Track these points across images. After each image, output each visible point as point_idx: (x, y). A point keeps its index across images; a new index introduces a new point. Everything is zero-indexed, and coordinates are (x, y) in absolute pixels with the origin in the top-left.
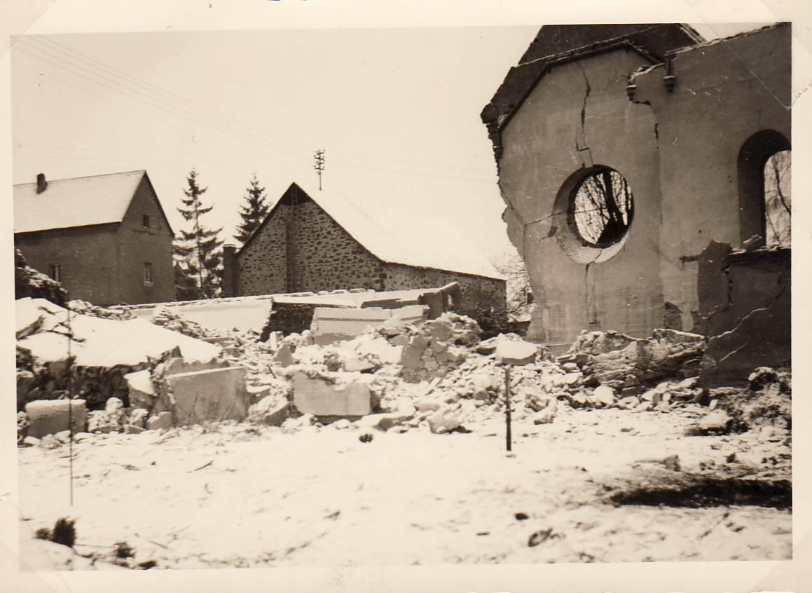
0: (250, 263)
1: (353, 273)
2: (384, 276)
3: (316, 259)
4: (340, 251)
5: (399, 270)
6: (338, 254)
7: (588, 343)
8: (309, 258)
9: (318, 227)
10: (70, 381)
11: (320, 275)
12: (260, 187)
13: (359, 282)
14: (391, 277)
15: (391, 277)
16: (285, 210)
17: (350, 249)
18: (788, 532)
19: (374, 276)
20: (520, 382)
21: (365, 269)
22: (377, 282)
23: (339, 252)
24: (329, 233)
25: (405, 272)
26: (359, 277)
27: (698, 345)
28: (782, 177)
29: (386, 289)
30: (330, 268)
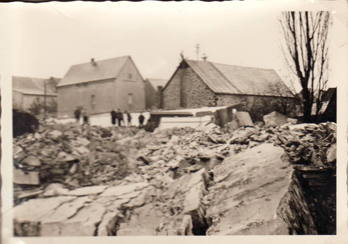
0: (168, 94)
1: (205, 98)
2: (217, 99)
3: (191, 92)
4: (201, 88)
5: (226, 96)
6: (200, 90)
7: (327, 163)
8: (189, 91)
9: (192, 78)
10: (298, 105)
11: (193, 99)
12: (206, 56)
13: (286, 93)
14: (221, 100)
15: (221, 100)
16: (180, 71)
17: (204, 87)
18: (96, 234)
19: (213, 100)
20: (112, 151)
21: (209, 96)
22: (214, 102)
23: (200, 89)
24: (196, 81)
25: (230, 96)
26: (207, 100)
27: (145, 191)
28: (101, 197)
29: (217, 105)
30: (196, 96)
